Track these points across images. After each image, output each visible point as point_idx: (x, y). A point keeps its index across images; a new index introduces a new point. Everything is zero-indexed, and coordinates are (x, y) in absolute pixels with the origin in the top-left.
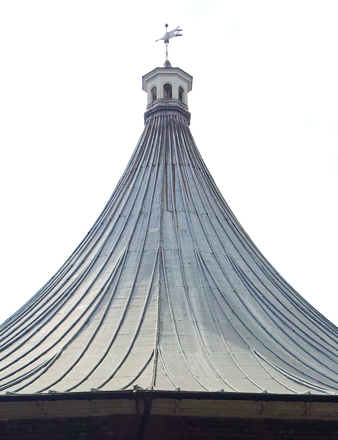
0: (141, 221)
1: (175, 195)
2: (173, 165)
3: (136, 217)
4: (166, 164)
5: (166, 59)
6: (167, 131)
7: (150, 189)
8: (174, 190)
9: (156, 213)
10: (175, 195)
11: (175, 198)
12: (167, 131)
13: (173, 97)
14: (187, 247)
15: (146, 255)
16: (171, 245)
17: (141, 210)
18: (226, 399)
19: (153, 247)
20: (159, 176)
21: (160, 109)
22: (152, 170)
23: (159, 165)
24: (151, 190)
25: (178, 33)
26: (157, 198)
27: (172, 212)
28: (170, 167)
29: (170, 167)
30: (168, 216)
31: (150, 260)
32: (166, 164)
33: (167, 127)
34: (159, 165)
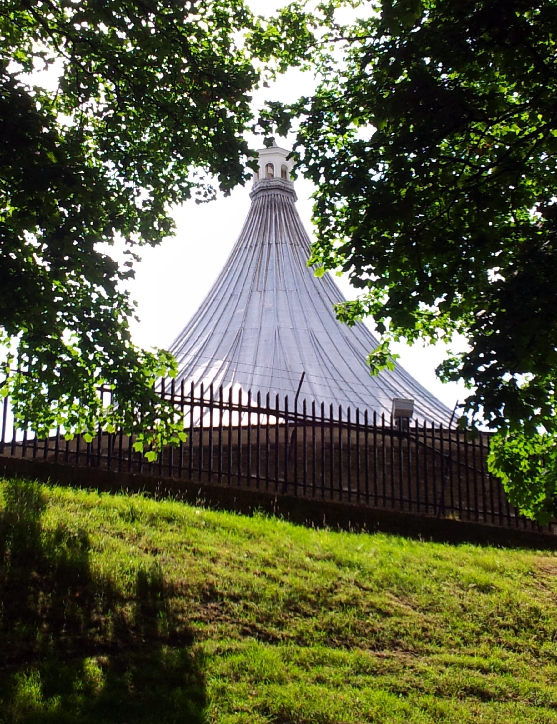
0: (230, 303)
1: (266, 275)
2: (270, 244)
3: (227, 299)
4: (263, 244)
5: (131, 340)
6: (267, 211)
7: (244, 271)
8: (267, 270)
9: (246, 294)
10: (266, 275)
11: (266, 278)
12: (267, 211)
13: (275, 176)
14: (269, 325)
15: (227, 336)
16: (253, 324)
17: (233, 292)
18: (191, 500)
19: (235, 328)
20: (255, 257)
21: (262, 189)
22: (249, 251)
23: (256, 245)
24: (245, 271)
25: (139, 321)
26: (250, 280)
27: (261, 291)
28: (266, 247)
29: (266, 247)
30: (256, 295)
31: (229, 341)
32: (263, 244)
33: (268, 206)
34: (256, 245)
